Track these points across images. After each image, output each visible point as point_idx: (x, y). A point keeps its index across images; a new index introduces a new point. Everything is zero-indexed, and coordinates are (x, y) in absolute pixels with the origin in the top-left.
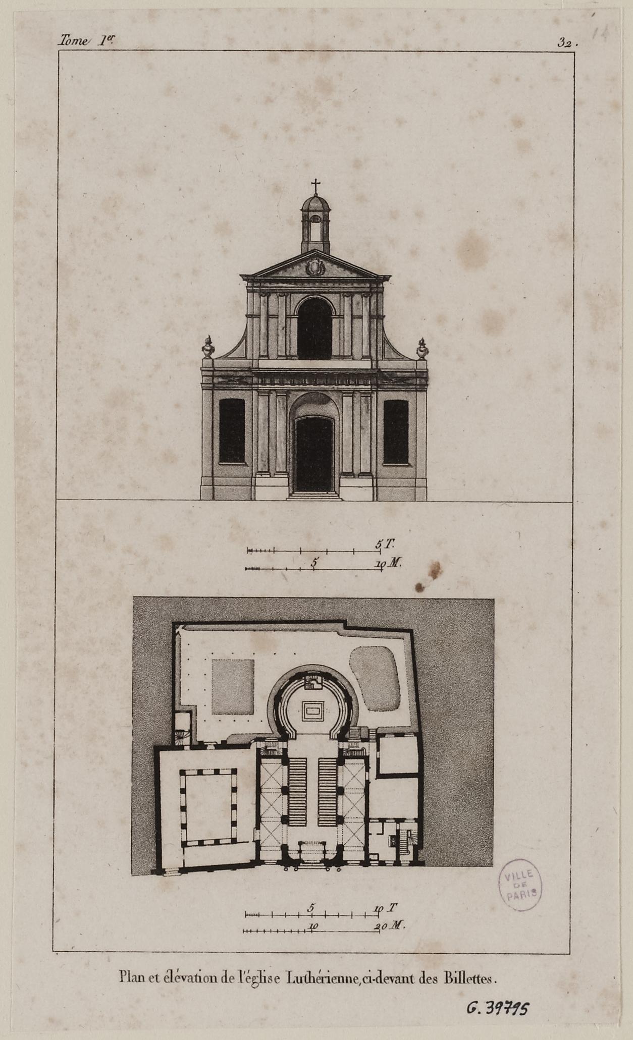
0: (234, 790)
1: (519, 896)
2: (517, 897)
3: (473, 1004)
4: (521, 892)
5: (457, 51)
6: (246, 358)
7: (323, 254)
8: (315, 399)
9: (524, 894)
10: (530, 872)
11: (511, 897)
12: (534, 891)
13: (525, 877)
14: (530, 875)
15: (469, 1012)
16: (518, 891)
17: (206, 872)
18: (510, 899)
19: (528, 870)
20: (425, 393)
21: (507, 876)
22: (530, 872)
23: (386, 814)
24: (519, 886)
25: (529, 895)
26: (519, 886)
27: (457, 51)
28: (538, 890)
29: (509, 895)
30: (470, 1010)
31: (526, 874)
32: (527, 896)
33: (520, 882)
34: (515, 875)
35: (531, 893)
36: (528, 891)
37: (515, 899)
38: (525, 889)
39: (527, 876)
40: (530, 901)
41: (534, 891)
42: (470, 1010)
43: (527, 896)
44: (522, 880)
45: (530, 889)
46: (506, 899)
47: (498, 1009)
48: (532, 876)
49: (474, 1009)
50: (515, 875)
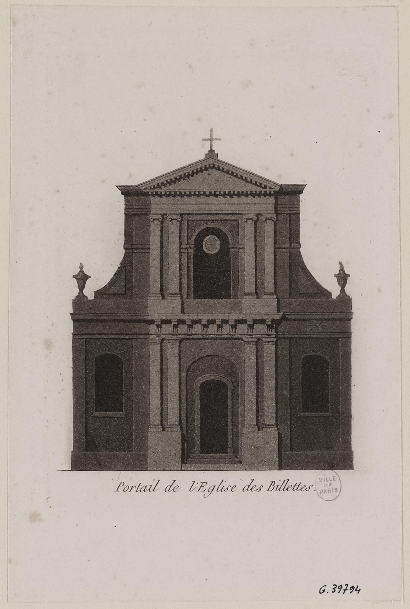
1: (327, 491)
2: (326, 492)
3: (324, 587)
4: (328, 489)
5: (251, 484)
6: (188, 221)
7: (213, 140)
9: (330, 491)
10: (334, 477)
11: (322, 492)
12: (336, 489)
13: (331, 481)
14: (334, 479)
16: (326, 488)
18: (322, 493)
19: (333, 477)
22: (334, 477)
23: (131, 473)
24: (327, 486)
25: (333, 491)
26: (327, 486)
27: (251, 484)
28: (339, 490)
29: (321, 491)
30: (321, 591)
31: (332, 479)
32: (332, 492)
33: (328, 483)
34: (325, 479)
35: (334, 490)
36: (332, 489)
37: (324, 493)
38: (331, 488)
39: (329, 480)
41: (336, 489)
43: (332, 492)
45: (334, 487)
47: (339, 589)
48: (335, 480)
49: (324, 591)
50: (325, 479)
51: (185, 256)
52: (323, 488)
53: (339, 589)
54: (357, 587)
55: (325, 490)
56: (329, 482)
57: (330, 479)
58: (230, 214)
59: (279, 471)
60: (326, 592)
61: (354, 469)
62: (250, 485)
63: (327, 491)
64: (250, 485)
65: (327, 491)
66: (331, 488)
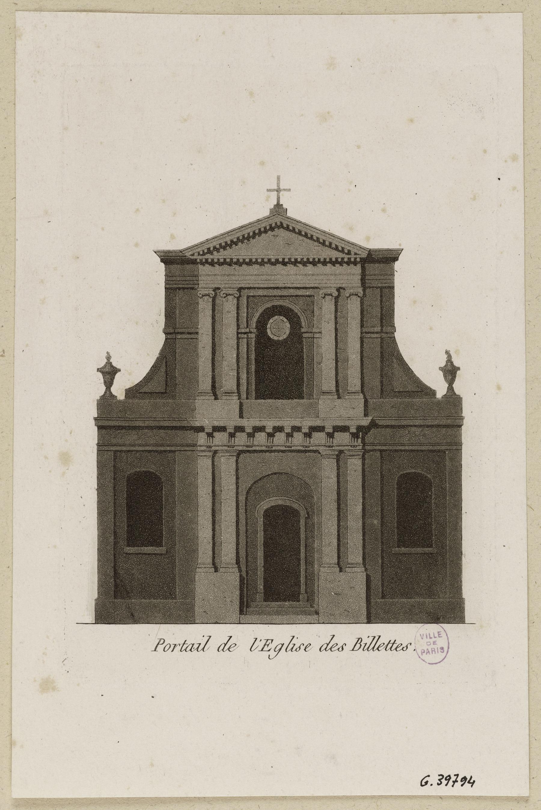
0: (533, 778)
1: (430, 652)
8: (211, 296)
9: (434, 651)
10: (439, 633)
12: (442, 648)
14: (440, 636)
15: (422, 785)
17: (396, 335)
19: (438, 632)
20: (94, 622)
21: (422, 635)
28: (446, 649)
29: (423, 651)
30: (423, 784)
31: (436, 635)
35: (439, 650)
36: (437, 648)
38: (435, 647)
40: (439, 656)
41: (442, 648)
42: (423, 784)
44: (434, 639)
46: (420, 654)
47: (447, 781)
49: (426, 783)
53: (447, 781)
56: (434, 639)
66: (435, 647)
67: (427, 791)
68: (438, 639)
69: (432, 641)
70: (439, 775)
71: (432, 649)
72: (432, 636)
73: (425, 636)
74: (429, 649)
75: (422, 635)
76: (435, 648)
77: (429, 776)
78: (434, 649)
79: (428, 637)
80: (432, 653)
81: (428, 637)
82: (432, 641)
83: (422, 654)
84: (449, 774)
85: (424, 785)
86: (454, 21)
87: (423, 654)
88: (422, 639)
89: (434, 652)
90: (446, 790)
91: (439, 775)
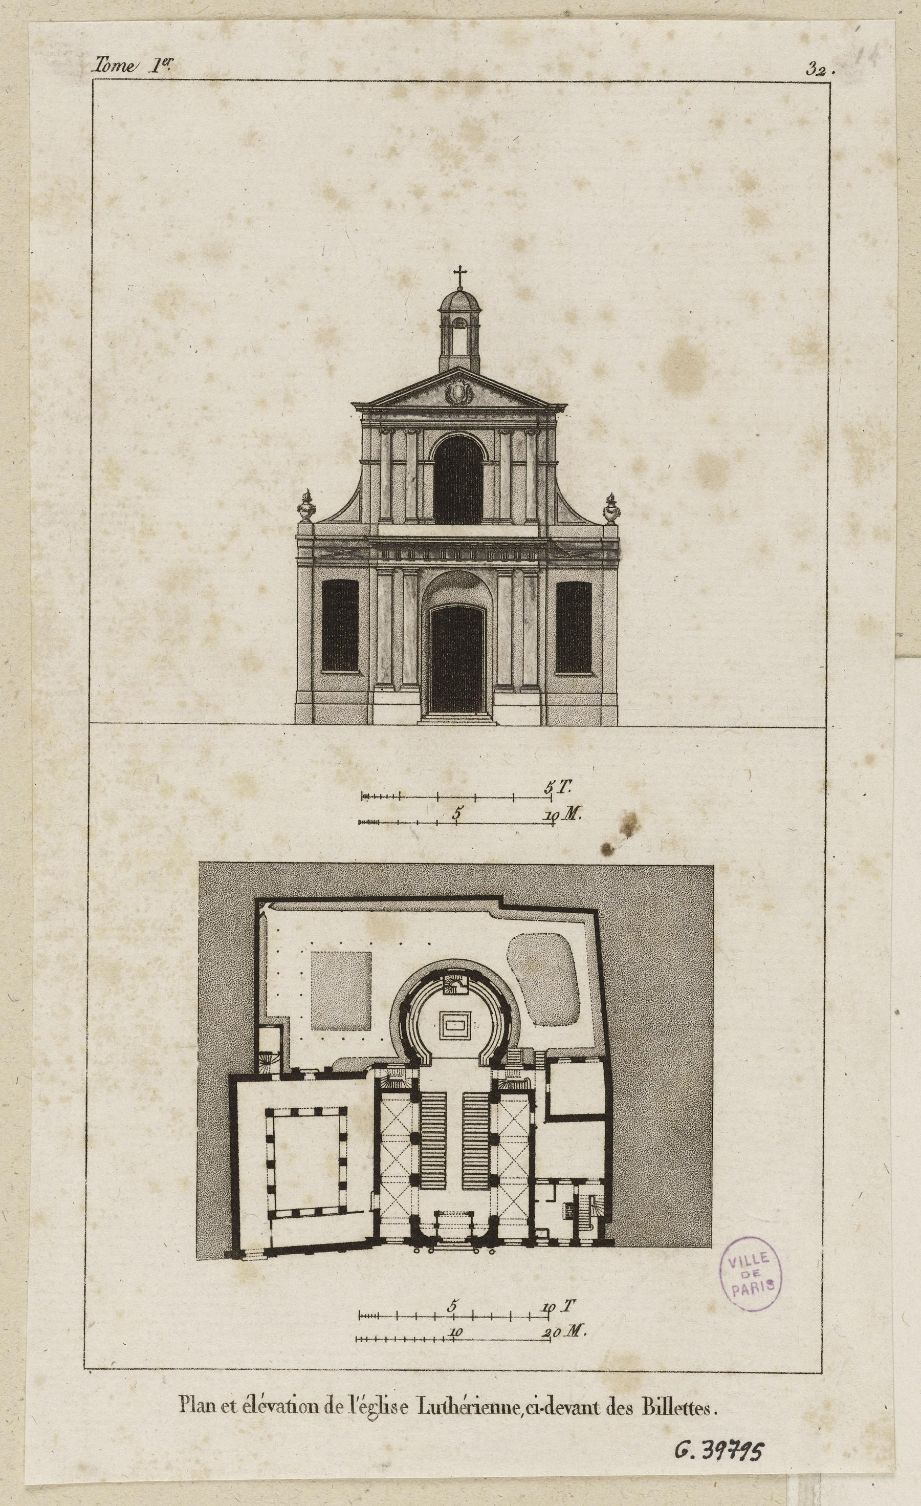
10: (764, 1255)
11: (738, 1291)
14: (764, 1259)
15: (678, 1456)
19: (762, 1253)
21: (732, 1261)
26: (749, 1275)
30: (680, 1453)
31: (758, 1259)
34: (743, 1260)
35: (765, 1285)
38: (758, 1280)
39: (753, 1263)
41: (770, 1282)
42: (680, 1453)
44: (755, 1267)
46: (730, 1294)
47: (719, 1452)
48: (767, 1261)
49: (685, 1452)
50: (743, 1260)
51: (384, 690)
52: (740, 1282)
53: (719, 1452)
54: (779, 1471)
55: (744, 1285)
56: (755, 1267)
57: (754, 1261)
58: (538, 649)
59: (557, 1177)
60: (689, 1455)
61: (323, 1114)
62: (825, 83)
63: (749, 1288)
64: (825, 83)
65: (749, 1288)
66: (758, 1280)
67: (684, 1466)
68: (762, 1267)
69: (750, 1270)
70: (704, 1442)
71: (752, 1284)
72: (750, 1260)
73: (738, 1262)
74: (746, 1285)
75: (732, 1261)
76: (757, 1282)
77: (689, 1442)
78: (756, 1283)
79: (744, 1263)
80: (753, 1292)
81: (744, 1263)
82: (750, 1270)
83: (734, 1295)
84: (264, 1111)
85: (681, 1456)
86: (848, 121)
87: (737, 1294)
88: (733, 1267)
89: (755, 1290)
90: (713, 1467)
91: (704, 1442)
